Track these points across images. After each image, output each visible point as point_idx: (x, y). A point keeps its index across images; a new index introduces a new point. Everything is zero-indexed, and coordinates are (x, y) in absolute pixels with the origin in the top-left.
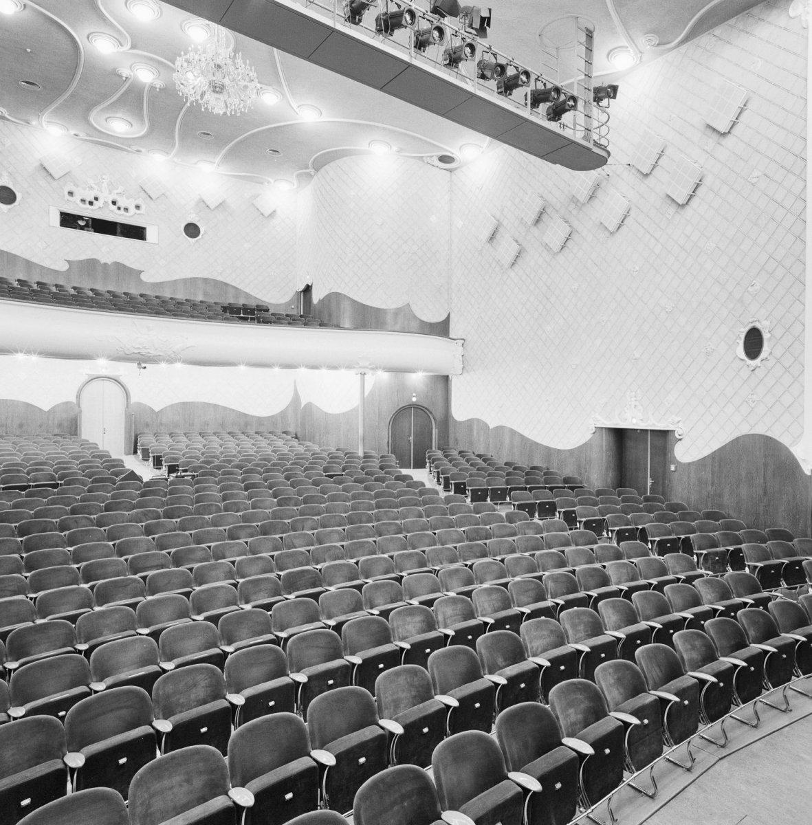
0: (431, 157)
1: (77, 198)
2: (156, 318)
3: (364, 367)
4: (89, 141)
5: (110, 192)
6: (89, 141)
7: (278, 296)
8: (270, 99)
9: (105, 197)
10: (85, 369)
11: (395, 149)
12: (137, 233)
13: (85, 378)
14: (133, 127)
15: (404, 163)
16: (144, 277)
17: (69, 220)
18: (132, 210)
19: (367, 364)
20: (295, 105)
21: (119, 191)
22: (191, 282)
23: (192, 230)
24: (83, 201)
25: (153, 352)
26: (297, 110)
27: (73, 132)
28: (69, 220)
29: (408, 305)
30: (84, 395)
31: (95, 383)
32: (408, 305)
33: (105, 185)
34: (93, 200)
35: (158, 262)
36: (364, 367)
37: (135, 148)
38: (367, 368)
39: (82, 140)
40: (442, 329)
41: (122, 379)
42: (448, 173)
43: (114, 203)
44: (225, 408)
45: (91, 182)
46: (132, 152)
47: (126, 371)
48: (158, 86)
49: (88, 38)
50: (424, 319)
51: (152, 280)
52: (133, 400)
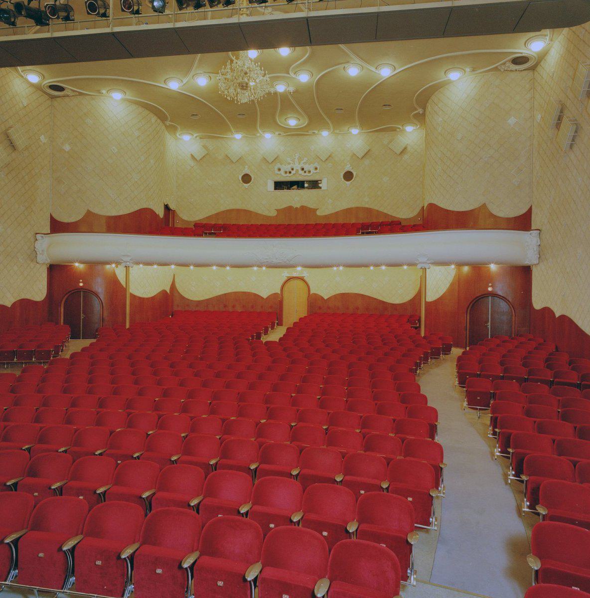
0: (504, 64)
1: (282, 172)
2: (460, 231)
3: (424, 263)
4: (287, 135)
5: (299, 163)
6: (287, 135)
7: (405, 213)
8: (353, 71)
9: (297, 167)
10: (286, 273)
11: (468, 70)
12: (315, 184)
13: (285, 279)
14: (301, 121)
15: (481, 79)
16: (318, 213)
17: (279, 185)
18: (313, 171)
19: (425, 260)
20: (373, 69)
21: (305, 161)
22: (349, 211)
23: (348, 176)
24: (286, 172)
25: (291, 263)
26: (22, 74)
27: (277, 133)
28: (279, 185)
29: (485, 204)
30: (285, 289)
31: (292, 282)
32: (485, 204)
33: (296, 160)
34: (291, 170)
35: (327, 202)
36: (424, 263)
37: (310, 132)
38: (426, 263)
39: (284, 136)
40: (523, 222)
41: (305, 278)
42: (530, 73)
43: (303, 169)
44: (369, 297)
45: (289, 160)
46: (311, 135)
47: (306, 273)
48: (292, 91)
49: (445, 73)
50: (501, 214)
51: (324, 214)
52: (312, 292)
